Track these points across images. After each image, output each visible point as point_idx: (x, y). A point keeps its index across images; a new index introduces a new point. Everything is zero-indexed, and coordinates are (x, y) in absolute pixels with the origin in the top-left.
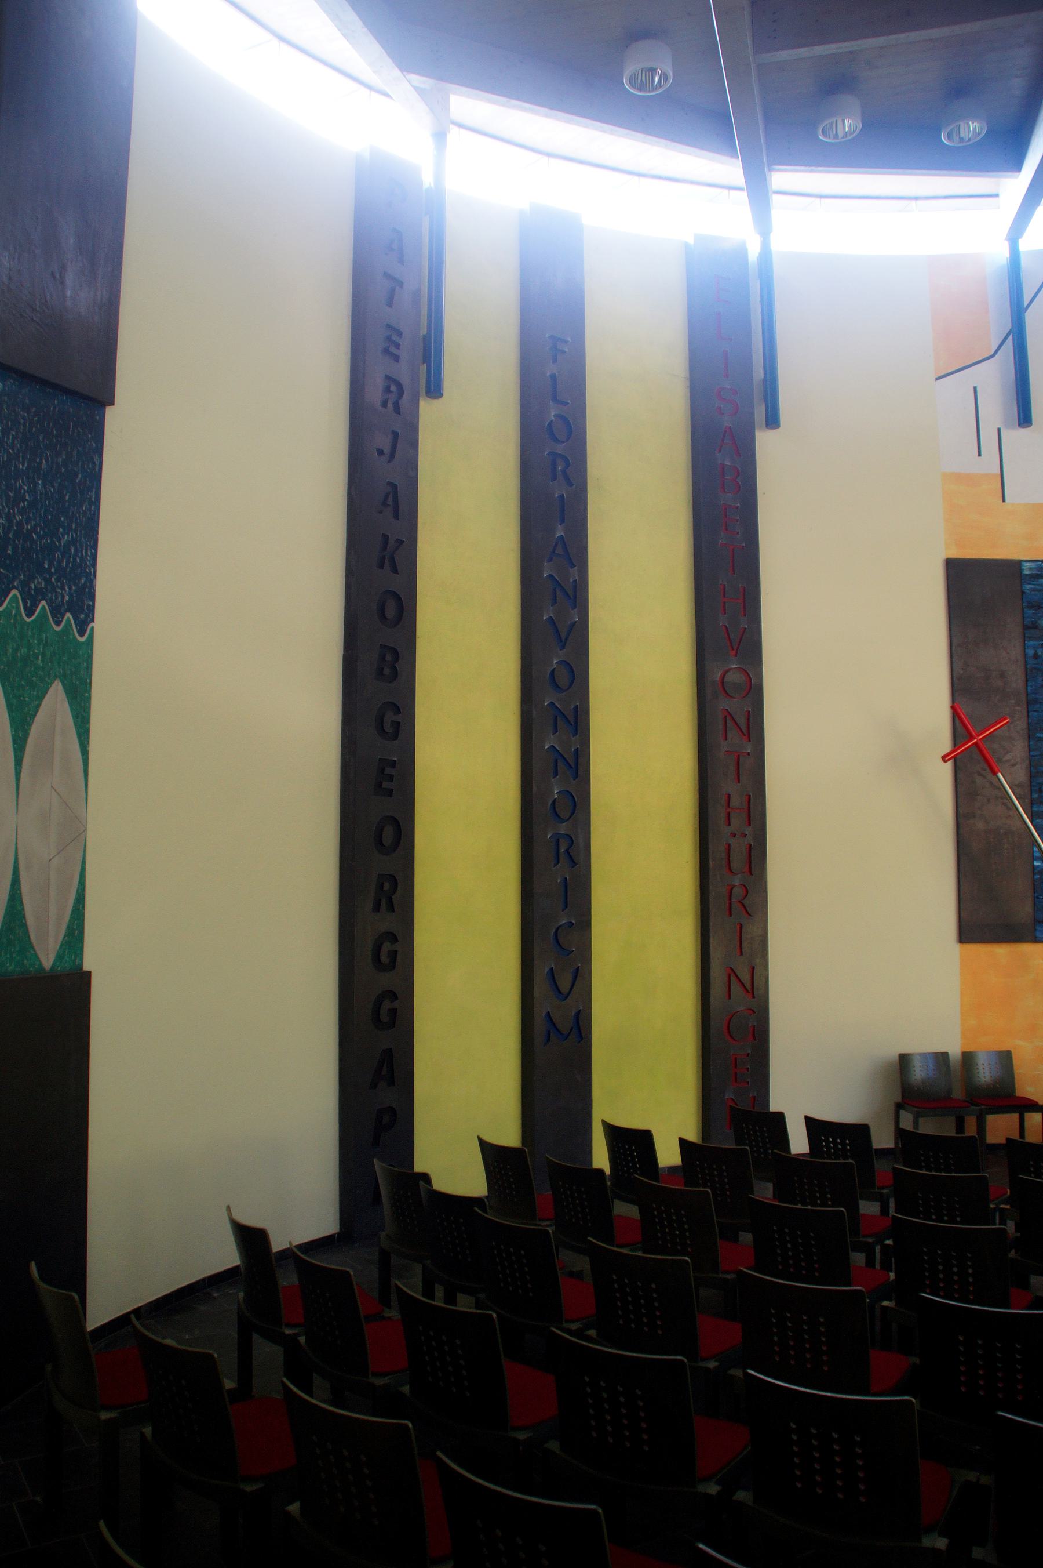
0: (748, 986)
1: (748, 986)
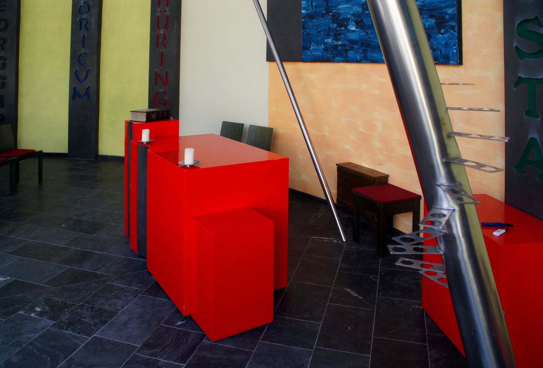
0: (158, 77)
1: (495, 170)
